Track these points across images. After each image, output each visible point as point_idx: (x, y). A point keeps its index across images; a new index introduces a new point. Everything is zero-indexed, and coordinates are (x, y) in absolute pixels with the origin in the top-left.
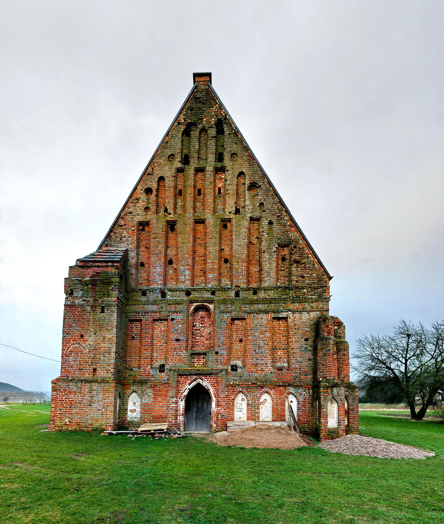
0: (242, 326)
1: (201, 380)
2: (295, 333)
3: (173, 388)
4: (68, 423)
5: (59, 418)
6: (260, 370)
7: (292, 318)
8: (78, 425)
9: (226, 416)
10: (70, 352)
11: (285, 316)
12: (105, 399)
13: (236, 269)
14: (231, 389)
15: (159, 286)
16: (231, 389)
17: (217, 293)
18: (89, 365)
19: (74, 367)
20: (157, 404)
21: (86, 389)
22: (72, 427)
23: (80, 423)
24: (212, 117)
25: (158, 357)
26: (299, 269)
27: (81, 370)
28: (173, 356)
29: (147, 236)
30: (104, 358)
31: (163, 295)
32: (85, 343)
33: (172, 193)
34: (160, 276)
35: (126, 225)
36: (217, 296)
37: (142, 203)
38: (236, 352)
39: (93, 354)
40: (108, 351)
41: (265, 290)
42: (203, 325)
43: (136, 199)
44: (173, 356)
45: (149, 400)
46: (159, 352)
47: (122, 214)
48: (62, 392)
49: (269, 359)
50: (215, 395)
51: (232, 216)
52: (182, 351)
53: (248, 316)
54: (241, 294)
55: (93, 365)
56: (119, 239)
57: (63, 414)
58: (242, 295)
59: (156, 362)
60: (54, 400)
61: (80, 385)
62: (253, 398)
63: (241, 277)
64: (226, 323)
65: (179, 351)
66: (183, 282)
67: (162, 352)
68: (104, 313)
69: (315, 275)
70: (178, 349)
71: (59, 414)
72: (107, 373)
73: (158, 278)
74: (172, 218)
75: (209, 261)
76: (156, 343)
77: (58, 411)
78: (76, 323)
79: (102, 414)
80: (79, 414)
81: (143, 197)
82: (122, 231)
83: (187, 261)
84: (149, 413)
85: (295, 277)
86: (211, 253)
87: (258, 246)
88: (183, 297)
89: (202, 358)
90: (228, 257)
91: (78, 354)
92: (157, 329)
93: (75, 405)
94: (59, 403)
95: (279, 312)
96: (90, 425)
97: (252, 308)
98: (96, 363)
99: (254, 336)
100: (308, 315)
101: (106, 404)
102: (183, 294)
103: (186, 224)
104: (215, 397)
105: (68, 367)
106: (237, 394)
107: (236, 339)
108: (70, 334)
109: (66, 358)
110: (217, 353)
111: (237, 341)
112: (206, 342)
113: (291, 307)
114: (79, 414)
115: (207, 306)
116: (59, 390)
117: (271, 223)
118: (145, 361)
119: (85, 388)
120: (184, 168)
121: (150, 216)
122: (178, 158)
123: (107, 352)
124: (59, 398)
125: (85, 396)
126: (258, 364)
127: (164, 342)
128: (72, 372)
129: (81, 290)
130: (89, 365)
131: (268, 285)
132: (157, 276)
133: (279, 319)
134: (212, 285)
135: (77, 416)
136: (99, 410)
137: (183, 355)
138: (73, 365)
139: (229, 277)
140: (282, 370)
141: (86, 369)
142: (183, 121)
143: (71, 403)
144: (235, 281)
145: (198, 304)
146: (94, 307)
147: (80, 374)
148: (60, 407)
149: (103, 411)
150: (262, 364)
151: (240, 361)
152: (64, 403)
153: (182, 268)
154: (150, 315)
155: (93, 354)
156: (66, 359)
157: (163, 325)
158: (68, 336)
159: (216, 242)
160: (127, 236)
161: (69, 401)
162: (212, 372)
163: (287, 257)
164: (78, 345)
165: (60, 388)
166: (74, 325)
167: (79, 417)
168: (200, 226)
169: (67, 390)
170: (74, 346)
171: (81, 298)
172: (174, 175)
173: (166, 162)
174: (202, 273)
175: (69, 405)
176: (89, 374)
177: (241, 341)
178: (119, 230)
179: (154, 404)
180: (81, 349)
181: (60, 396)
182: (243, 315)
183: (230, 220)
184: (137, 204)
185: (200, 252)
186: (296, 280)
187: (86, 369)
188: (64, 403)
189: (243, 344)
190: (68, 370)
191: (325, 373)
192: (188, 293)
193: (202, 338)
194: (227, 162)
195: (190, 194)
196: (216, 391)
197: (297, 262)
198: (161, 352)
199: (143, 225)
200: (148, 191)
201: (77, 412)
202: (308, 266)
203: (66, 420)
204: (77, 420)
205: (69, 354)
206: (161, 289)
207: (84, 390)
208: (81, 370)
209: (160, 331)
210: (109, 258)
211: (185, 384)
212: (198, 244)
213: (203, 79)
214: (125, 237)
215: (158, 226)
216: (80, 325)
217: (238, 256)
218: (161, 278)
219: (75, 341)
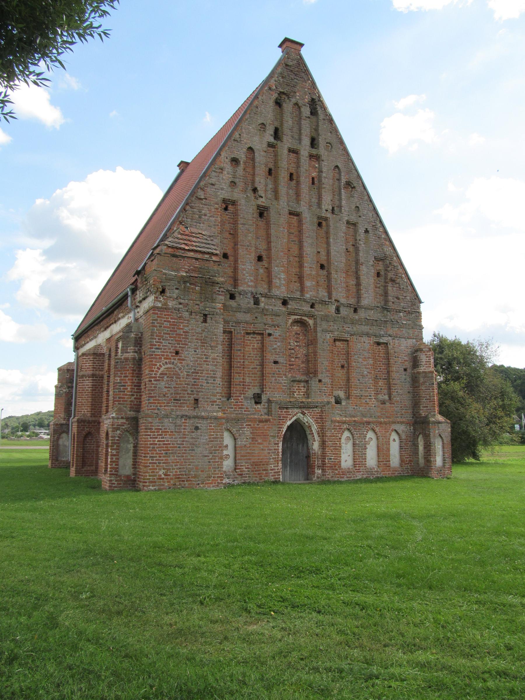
0: (343, 349)
1: (301, 415)
2: (396, 362)
3: (275, 425)
4: (163, 476)
5: (150, 469)
6: (364, 404)
7: (391, 344)
8: (179, 478)
9: (334, 459)
10: (161, 374)
11: (385, 341)
12: (212, 441)
13: (335, 279)
14: (338, 426)
15: (250, 289)
16: (338, 426)
17: (316, 306)
18: (188, 394)
19: (168, 397)
20: (256, 447)
21: (187, 427)
22: (169, 482)
23: (181, 475)
24: (305, 94)
25: (251, 383)
26: (394, 289)
27: (177, 400)
28: (271, 383)
29: (232, 218)
30: (208, 385)
31: (257, 302)
32: (181, 363)
33: (263, 171)
34: (250, 276)
35: (206, 199)
36: (317, 311)
37: (227, 175)
38: (338, 380)
39: (194, 379)
40: (212, 375)
41: (365, 309)
42: (298, 344)
43: (220, 169)
44: (271, 383)
45: (247, 441)
46: (252, 377)
47: (202, 184)
48: (154, 432)
49: (373, 391)
50: (318, 434)
51: (329, 215)
52: (281, 377)
53: (351, 337)
54: (341, 309)
55: (193, 394)
56: (197, 216)
57: (156, 463)
58: (344, 311)
59: (249, 390)
60: (115, 443)
62: (359, 436)
63: (340, 290)
64: (329, 345)
65: (278, 377)
66: (279, 288)
67: (256, 377)
68: (206, 323)
69: (408, 298)
70: (277, 374)
71: (150, 463)
72: (212, 405)
73: (248, 278)
74: (264, 203)
75: (306, 265)
76: (248, 365)
77: (149, 460)
78: (169, 334)
79: (209, 462)
80: (178, 462)
81: (228, 168)
82: (201, 206)
83: (282, 262)
84: (247, 459)
85: (391, 298)
86: (308, 254)
87: (354, 255)
88: (279, 308)
89: (302, 387)
90: (325, 263)
91: (173, 377)
92: (248, 346)
93: (172, 450)
94: (149, 447)
95: (381, 336)
96: (194, 477)
97: (355, 329)
98: (197, 391)
99: (358, 362)
100: (405, 342)
101: (213, 448)
102: (279, 303)
103: (280, 214)
104: (319, 436)
105: (159, 397)
106: (343, 432)
107: (338, 364)
108: (161, 349)
109: (155, 382)
110: (320, 381)
111: (339, 367)
112: (302, 366)
113: (390, 332)
114: (178, 462)
115: (305, 320)
116: (150, 429)
117: (367, 231)
118: (237, 388)
119: (186, 426)
120: (277, 144)
121: (237, 195)
122: (270, 131)
123: (211, 377)
124: (150, 441)
125: (186, 438)
126: (362, 396)
127: (258, 364)
129: (177, 289)
130: (188, 394)
131: (367, 302)
132: (247, 275)
133: (378, 344)
134: (310, 295)
135: (175, 466)
136: (206, 456)
137: (283, 382)
138: (166, 394)
139: (326, 287)
140: (385, 403)
141: (184, 400)
142: (274, 88)
143: (167, 447)
144: (334, 294)
145: (296, 317)
146: (193, 314)
148: (152, 454)
149: (210, 457)
150: (366, 396)
151: (342, 392)
152: (157, 448)
153: (276, 268)
154: (243, 327)
155: (194, 379)
156: (156, 384)
157: (257, 340)
158: (158, 352)
159: (313, 243)
160: (208, 215)
161: (164, 444)
162: (317, 405)
163: (382, 273)
167: (179, 466)
168: (294, 218)
170: (167, 366)
172: (265, 149)
173: (256, 131)
174: (297, 279)
175: (164, 450)
177: (343, 367)
178: (197, 204)
179: (254, 447)
180: (176, 371)
181: (151, 438)
182: (346, 336)
183: (326, 219)
184: (221, 175)
185: (294, 252)
186: (392, 300)
187: (184, 400)
188: (157, 448)
189: (345, 371)
190: (159, 400)
191: (429, 408)
192: (285, 303)
193: (297, 360)
194: (322, 151)
195: (284, 178)
196: (320, 428)
197: (393, 281)
198: (254, 377)
199: (227, 204)
200: (235, 161)
201: (176, 459)
202: (402, 287)
203: (161, 473)
204: (176, 472)
206: (252, 293)
207: (184, 429)
208: (177, 400)
209: (252, 349)
210: (203, 247)
211: (286, 420)
212: (292, 241)
214: (205, 215)
215: (247, 209)
217: (336, 264)
218: (252, 278)
219: (167, 359)
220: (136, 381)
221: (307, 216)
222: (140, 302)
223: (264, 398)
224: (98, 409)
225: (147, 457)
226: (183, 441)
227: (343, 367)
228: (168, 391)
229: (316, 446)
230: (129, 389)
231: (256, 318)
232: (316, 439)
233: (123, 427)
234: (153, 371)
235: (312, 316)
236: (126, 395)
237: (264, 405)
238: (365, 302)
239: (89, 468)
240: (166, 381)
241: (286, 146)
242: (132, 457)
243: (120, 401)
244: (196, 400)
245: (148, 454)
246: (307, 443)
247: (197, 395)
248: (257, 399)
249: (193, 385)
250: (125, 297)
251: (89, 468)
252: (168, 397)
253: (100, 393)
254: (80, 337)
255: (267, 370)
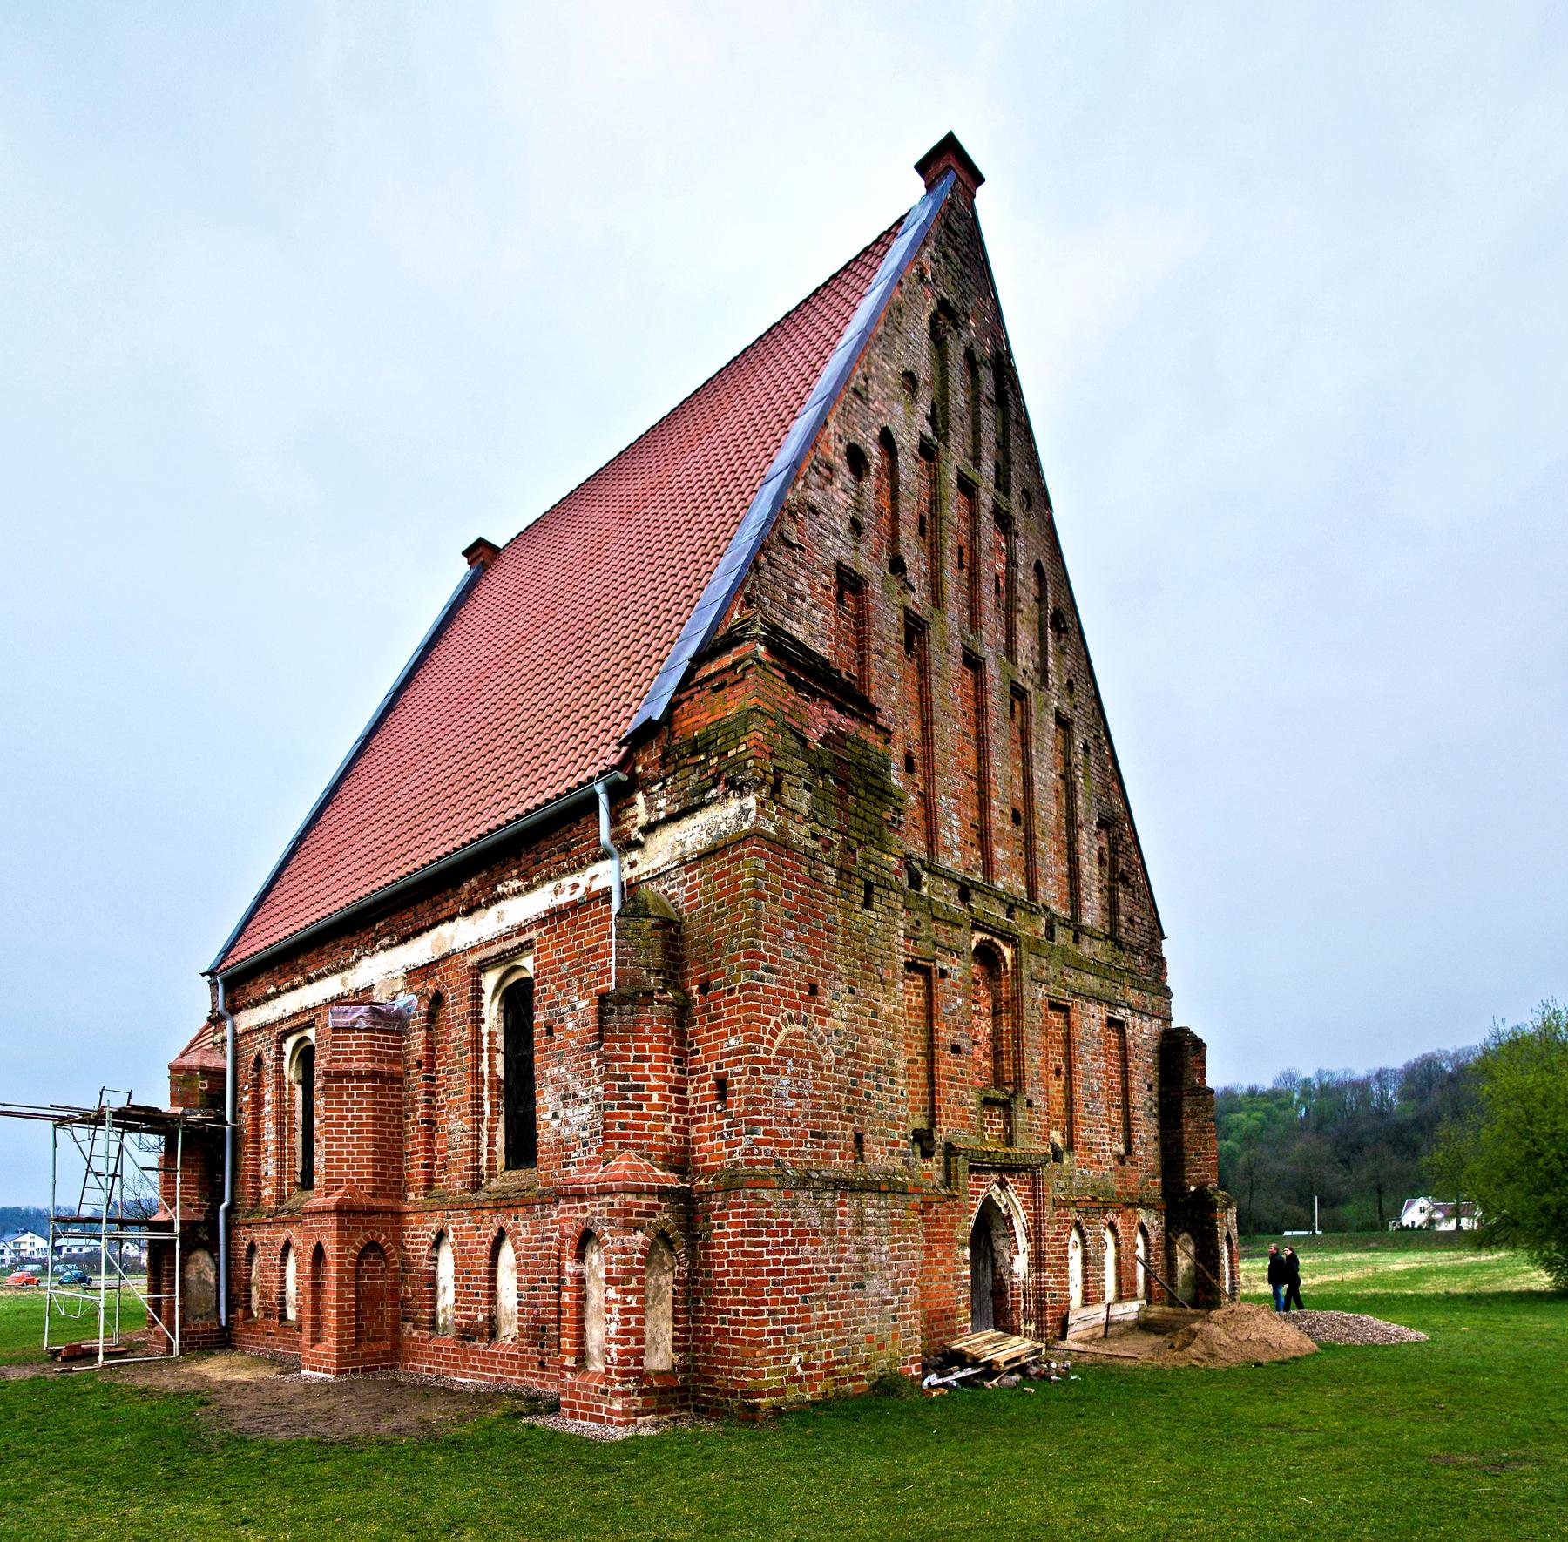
4: (800, 1370)
5: (772, 1352)
18: (841, 1117)
19: (798, 1125)
22: (813, 1388)
23: (838, 1362)
32: (822, 1022)
50: (1028, 1235)
60: (633, 1272)
61: (828, 1203)
71: (771, 1333)
77: (765, 1323)
93: (818, 1288)
104: (1029, 1241)
109: (767, 1078)
121: (869, 566)
128: (790, 1144)
129: (808, 787)
130: (841, 1117)
147: (816, 1155)
149: (896, 1304)
152: (785, 1282)
156: (770, 1083)
161: (799, 1271)
164: (800, 1028)
165: (769, 1214)
166: (790, 934)
169: (791, 1225)
171: (806, 819)
176: (842, 1156)
181: (768, 1253)
187: (834, 1136)
188: (785, 1282)
201: (827, 1317)
205: (776, 1061)
213: (948, 165)
216: (806, 941)
220: (674, 1076)
221: (994, 673)
222: (649, 829)
223: (939, 1139)
224: (392, 1175)
225: (761, 1313)
226: (840, 1260)
227: (1058, 1072)
228: (798, 1105)
229: (1021, 1264)
230: (655, 1099)
231: (918, 923)
232: (1021, 1249)
233: (653, 1220)
234: (761, 1040)
235: (1010, 939)
236: (647, 1117)
237: (938, 1162)
238: (1087, 920)
239: (374, 1347)
240: (793, 1075)
241: (955, 464)
242: (670, 1313)
243: (627, 1137)
244: (859, 1139)
245: (765, 1302)
246: (994, 1261)
247: (861, 1121)
248: (923, 1140)
249: (851, 1092)
250: (579, 809)
251: (374, 1347)
252: (798, 1125)
253: (396, 1127)
254: (238, 981)
255: (941, 1069)
